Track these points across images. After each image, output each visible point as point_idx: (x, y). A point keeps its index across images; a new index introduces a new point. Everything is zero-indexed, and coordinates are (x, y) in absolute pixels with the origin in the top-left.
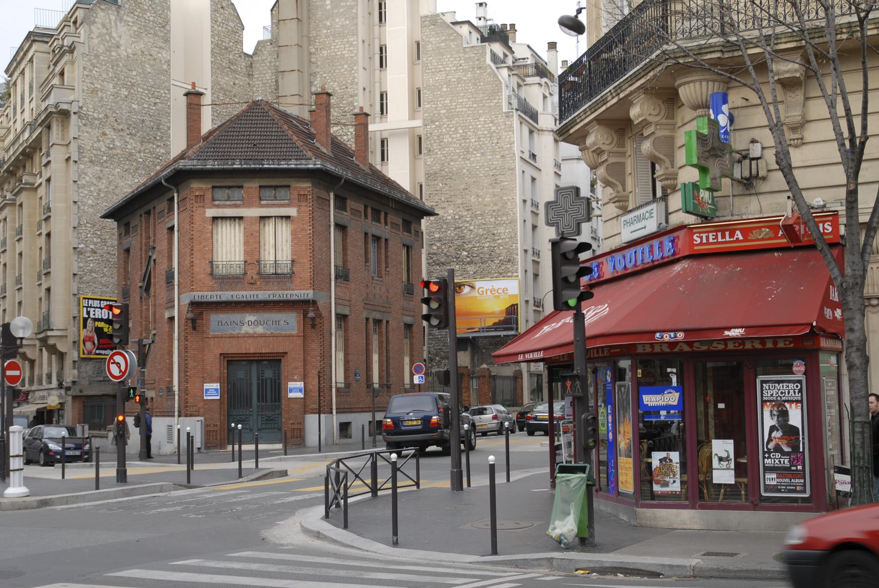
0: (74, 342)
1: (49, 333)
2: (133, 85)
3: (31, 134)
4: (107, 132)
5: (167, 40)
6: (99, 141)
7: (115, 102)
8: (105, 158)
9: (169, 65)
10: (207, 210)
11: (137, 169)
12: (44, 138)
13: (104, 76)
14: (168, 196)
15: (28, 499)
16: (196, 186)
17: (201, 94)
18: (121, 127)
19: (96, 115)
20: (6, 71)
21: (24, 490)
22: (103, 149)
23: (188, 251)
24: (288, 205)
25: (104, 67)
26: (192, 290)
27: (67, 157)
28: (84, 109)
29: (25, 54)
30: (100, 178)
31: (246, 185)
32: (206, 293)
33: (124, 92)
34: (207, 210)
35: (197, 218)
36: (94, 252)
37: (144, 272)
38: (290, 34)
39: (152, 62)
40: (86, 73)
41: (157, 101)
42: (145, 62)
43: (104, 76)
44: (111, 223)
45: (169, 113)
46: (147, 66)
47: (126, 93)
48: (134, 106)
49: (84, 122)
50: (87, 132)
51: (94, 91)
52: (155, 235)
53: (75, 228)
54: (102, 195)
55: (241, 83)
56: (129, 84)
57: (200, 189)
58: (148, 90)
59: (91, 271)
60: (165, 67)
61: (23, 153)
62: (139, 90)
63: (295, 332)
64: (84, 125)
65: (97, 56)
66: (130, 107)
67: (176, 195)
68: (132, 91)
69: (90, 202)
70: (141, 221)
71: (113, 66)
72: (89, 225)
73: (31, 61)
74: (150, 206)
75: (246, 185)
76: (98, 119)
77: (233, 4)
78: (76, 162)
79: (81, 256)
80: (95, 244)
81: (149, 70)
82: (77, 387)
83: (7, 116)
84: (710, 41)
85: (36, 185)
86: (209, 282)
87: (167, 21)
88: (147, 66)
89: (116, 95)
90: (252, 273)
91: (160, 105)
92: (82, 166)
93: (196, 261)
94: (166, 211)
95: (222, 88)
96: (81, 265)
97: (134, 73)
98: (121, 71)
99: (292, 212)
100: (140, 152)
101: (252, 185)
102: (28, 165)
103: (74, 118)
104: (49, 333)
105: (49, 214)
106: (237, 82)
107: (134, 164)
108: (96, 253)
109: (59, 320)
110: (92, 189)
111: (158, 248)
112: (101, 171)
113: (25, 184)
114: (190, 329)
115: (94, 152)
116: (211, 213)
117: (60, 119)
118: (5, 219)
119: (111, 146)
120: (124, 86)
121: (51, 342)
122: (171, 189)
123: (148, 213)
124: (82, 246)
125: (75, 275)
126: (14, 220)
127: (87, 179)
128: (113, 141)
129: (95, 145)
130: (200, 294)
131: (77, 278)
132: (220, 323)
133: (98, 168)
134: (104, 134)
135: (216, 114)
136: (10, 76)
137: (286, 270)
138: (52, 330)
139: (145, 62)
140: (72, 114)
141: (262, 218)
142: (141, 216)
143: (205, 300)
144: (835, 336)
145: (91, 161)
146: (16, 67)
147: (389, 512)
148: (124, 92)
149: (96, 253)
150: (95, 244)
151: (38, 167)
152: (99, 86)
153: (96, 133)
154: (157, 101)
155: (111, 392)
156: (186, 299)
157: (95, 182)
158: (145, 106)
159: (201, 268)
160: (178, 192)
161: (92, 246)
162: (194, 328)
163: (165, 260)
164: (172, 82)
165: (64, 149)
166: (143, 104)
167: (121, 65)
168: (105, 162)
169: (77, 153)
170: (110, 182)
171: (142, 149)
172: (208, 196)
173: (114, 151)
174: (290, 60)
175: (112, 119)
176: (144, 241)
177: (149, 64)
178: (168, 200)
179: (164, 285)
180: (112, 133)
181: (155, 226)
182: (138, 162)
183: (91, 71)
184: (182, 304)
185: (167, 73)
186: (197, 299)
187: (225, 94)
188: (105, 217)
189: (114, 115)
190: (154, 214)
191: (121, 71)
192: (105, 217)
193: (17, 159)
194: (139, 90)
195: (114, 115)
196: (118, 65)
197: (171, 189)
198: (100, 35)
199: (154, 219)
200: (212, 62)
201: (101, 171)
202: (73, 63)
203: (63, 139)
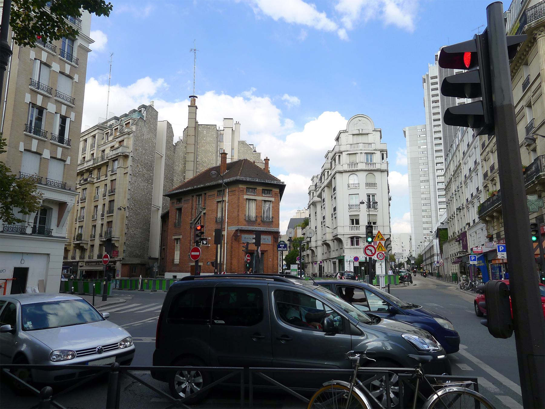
5: (156, 136)
24: (271, 197)
31: (258, 188)
35: (241, 198)
38: (191, 140)
44: (168, 199)
51: (136, 150)
52: (205, 203)
59: (131, 216)
63: (270, 243)
65: (138, 137)
75: (258, 188)
86: (245, 223)
87: (156, 130)
90: (259, 220)
93: (240, 214)
99: (273, 199)
101: (260, 188)
103: (130, 159)
114: (234, 240)
116: (246, 197)
132: (245, 238)
137: (254, 219)
140: (130, 157)
141: (265, 201)
142: (193, 196)
144: (422, 261)
156: (234, 228)
159: (242, 217)
172: (245, 190)
174: (191, 149)
198: (139, 130)
202: (129, 138)
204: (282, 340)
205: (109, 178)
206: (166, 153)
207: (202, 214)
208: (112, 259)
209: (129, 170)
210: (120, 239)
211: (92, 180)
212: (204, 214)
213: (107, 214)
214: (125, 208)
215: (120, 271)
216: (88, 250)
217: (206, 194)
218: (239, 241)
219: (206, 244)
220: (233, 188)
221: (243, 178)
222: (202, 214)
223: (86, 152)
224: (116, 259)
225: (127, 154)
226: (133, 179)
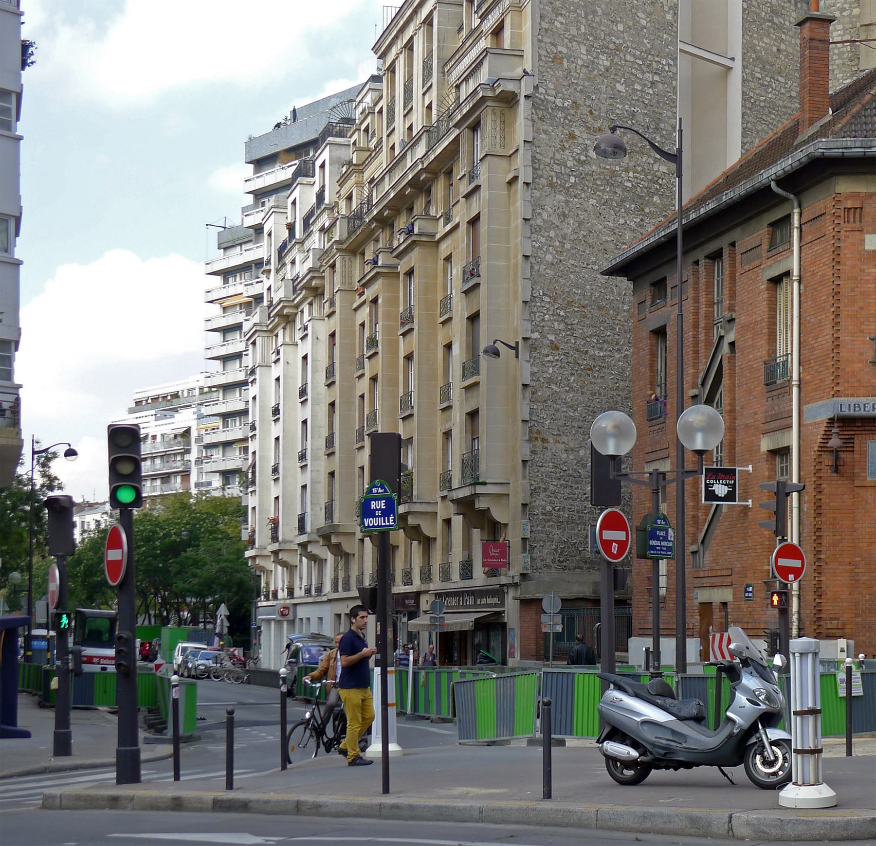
0: (524, 505)
1: (480, 489)
2: (617, 49)
3: (430, 149)
4: (577, 133)
6: (563, 148)
7: (589, 80)
8: (572, 180)
9: (675, 14)
10: (868, 237)
11: (623, 201)
12: (464, 148)
13: (574, 31)
14: (777, 214)
15: (838, 816)
16: (846, 187)
17: (829, 21)
18: (598, 125)
19: (559, 102)
20: (375, 49)
21: (824, 792)
22: (569, 164)
23: (827, 318)
25: (573, 16)
26: (837, 394)
27: (510, 176)
28: (541, 90)
29: (415, 12)
30: (564, 215)
32: (862, 400)
33: (604, 61)
34: (868, 237)
35: (847, 253)
36: (554, 347)
37: (703, 368)
39: (649, 9)
40: (545, 25)
41: (657, 78)
42: (637, 8)
43: (574, 31)
44: (624, 283)
45: (674, 102)
46: (640, 14)
47: (607, 63)
48: (620, 87)
49: (540, 113)
50: (545, 132)
51: (557, 59)
52: (733, 296)
53: (525, 302)
54: (568, 246)
55: (790, 50)
56: (612, 46)
57: (854, 196)
58: (643, 59)
59: (550, 381)
60: (669, 17)
61: (414, 183)
62: (628, 58)
64: (541, 119)
66: (613, 88)
67: (796, 211)
68: (616, 59)
69: (549, 257)
70: (696, 273)
71: (586, 15)
72: (547, 299)
73: (428, 22)
74: (723, 243)
76: (563, 109)
77: (20, 329)
78: (527, 184)
79: (535, 354)
80: (556, 333)
81: (644, 22)
82: (531, 585)
83: (366, 130)
84: (795, 230)
85: (438, 236)
88: (640, 14)
89: (590, 65)
91: (660, 86)
92: (537, 194)
93: (845, 338)
94: (765, 246)
95: (758, 58)
96: (535, 370)
97: (621, 27)
98: (600, 23)
100: (627, 170)
102: (419, 206)
103: (523, 107)
104: (480, 489)
105: (475, 280)
106: (783, 47)
107: (619, 191)
108: (557, 348)
109: (492, 468)
110: (552, 234)
111: (742, 319)
112: (567, 202)
113: (420, 235)
114: (827, 472)
115: (556, 168)
117: (498, 111)
118: (375, 301)
119: (583, 158)
120: (604, 49)
121: (481, 504)
122: (786, 200)
123: (716, 256)
124: (536, 335)
125: (525, 386)
126: (395, 302)
127: (545, 216)
128: (586, 149)
129: (558, 156)
130: (853, 400)
131: (529, 390)
133: (562, 198)
134: (572, 136)
135: (748, 105)
136: (383, 56)
138: (485, 484)
139: (637, 8)
140: (522, 99)
142: (697, 263)
143: (862, 413)
145: (551, 185)
146: (396, 37)
147: (223, 748)
148: (604, 61)
149: (557, 348)
150: (556, 333)
151: (441, 204)
152: (564, 50)
153: (559, 133)
154: (657, 78)
155: (586, 591)
156: (822, 411)
157: (556, 221)
158: (637, 86)
160: (800, 206)
161: (552, 337)
162: (836, 469)
163: (763, 341)
164: (680, 46)
165: (504, 163)
166: (633, 83)
167: (600, 12)
168: (573, 186)
169: (530, 170)
170: (581, 223)
171: (632, 164)
173: (587, 168)
175: (585, 110)
176: (703, 310)
177: (644, 12)
178: (773, 225)
179: (759, 388)
180: (585, 136)
181: (733, 279)
182: (625, 189)
183: (552, 22)
184: (807, 421)
185: (671, 27)
186: (846, 412)
187: (763, 68)
188: (612, 272)
189: (588, 102)
190: (733, 258)
191: (600, 23)
192: (612, 272)
193: (400, 195)
194: (628, 58)
195: (588, 102)
196: (594, 12)
197: (786, 200)
199: (733, 265)
200: (744, 10)
201: (567, 202)
203: (503, 146)
204: (68, 617)
205: (461, 215)
206: (748, 48)
207: (725, 349)
208: (494, 581)
209: (521, 165)
210: (510, 490)
211: (428, 227)
212: (732, 344)
213: (464, 376)
214: (516, 348)
215: (517, 631)
216: (439, 542)
217: (733, 244)
218: (852, 477)
219: (730, 496)
220: (820, 201)
221: (849, 141)
222: (725, 349)
223: (414, 103)
224: (504, 580)
225: (510, 87)
226: (549, 203)
